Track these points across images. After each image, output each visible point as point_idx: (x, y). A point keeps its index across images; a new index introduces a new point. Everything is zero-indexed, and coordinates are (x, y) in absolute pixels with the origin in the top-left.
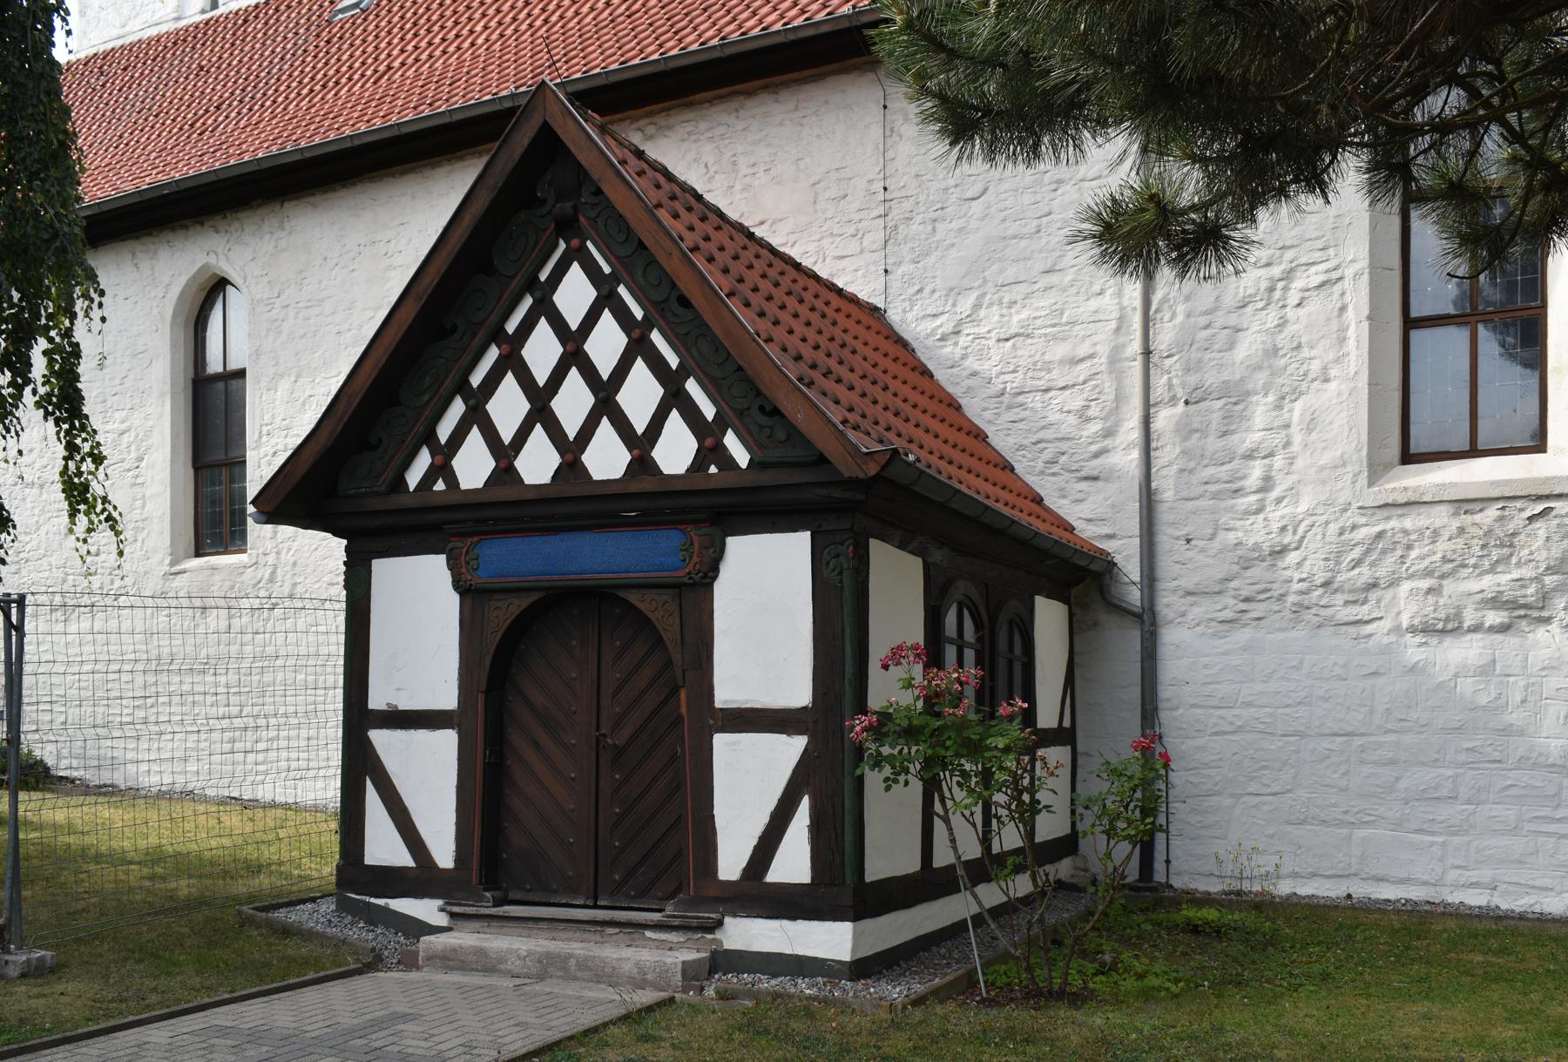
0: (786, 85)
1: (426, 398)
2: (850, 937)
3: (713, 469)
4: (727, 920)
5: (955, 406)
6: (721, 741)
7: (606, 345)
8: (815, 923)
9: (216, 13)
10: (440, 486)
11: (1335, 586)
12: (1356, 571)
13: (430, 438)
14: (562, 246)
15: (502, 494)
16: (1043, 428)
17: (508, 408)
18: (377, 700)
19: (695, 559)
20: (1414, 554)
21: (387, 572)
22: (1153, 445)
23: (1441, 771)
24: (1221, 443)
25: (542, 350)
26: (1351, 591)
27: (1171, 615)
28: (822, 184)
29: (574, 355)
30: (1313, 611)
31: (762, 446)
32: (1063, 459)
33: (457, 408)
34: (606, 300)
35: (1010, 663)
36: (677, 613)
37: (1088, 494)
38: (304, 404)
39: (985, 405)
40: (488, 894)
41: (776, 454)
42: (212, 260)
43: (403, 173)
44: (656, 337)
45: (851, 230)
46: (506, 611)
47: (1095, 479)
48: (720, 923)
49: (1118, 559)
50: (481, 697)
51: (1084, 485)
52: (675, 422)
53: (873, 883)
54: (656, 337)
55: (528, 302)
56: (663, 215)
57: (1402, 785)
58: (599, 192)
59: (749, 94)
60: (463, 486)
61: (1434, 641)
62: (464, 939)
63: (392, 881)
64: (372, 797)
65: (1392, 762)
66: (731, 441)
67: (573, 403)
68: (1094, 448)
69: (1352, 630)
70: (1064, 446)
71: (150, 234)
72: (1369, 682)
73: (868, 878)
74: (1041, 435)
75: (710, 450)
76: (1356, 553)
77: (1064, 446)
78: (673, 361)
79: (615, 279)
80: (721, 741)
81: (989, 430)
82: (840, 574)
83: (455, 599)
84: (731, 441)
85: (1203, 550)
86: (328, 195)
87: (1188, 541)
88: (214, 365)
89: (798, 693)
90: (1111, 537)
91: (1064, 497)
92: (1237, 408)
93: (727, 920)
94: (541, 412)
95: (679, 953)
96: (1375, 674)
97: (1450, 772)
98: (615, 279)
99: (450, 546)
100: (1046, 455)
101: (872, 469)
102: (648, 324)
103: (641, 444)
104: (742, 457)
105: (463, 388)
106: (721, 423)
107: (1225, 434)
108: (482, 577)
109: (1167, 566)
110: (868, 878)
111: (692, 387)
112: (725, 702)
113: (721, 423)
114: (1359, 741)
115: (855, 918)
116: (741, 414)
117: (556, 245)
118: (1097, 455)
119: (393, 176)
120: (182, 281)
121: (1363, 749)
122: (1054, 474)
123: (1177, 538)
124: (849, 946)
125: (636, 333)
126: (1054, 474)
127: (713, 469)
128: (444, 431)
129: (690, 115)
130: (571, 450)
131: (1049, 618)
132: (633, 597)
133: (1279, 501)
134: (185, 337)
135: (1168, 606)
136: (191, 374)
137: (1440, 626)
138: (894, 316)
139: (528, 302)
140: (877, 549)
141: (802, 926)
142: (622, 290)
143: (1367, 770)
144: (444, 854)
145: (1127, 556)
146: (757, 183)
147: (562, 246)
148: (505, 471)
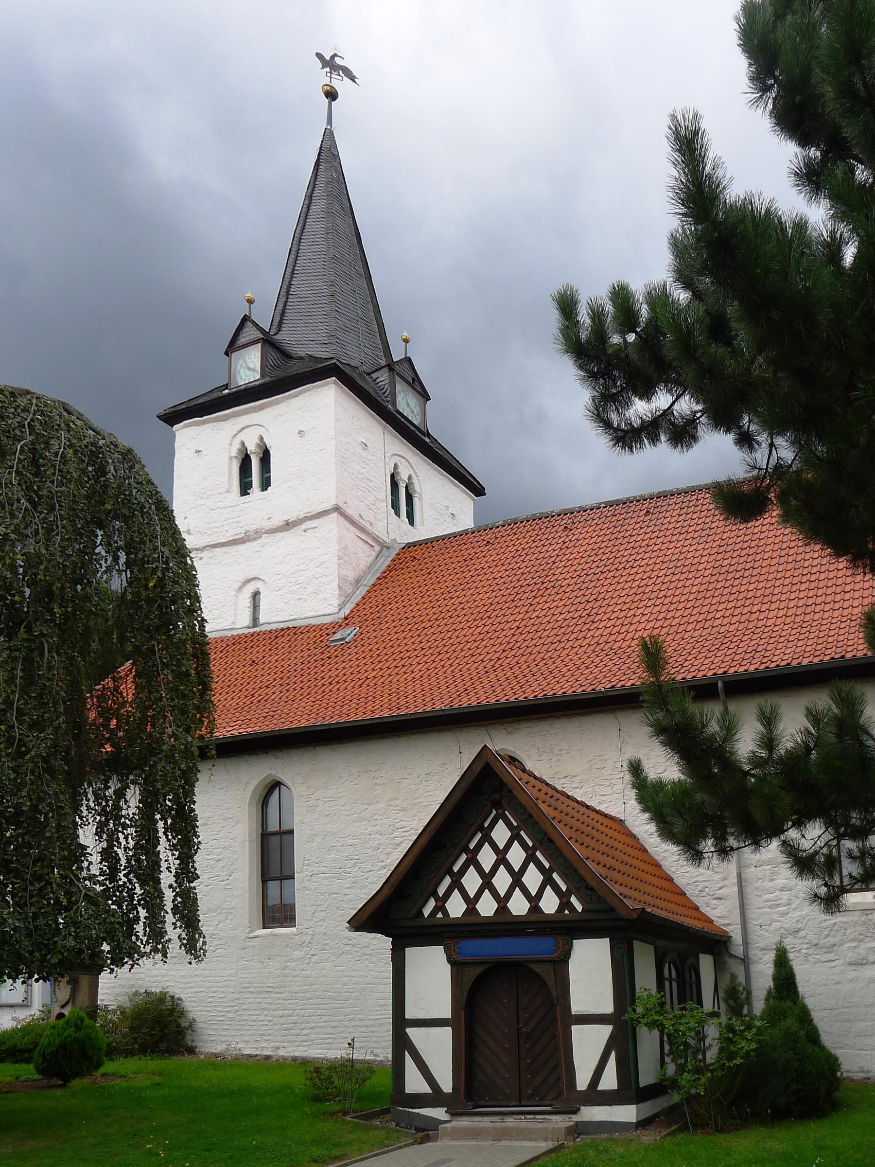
0: (575, 715)
1: (433, 876)
2: (635, 1111)
3: (567, 912)
4: (582, 1108)
5: (658, 866)
6: (574, 1028)
7: (516, 855)
8: (620, 1106)
9: (257, 629)
10: (440, 915)
11: (819, 946)
12: (827, 940)
13: (434, 894)
14: (494, 812)
15: (471, 920)
16: (697, 876)
17: (472, 881)
18: (410, 1014)
19: (560, 950)
20: (848, 932)
21: (413, 954)
22: (743, 884)
23: (867, 1023)
24: (771, 884)
25: (487, 857)
26: (826, 948)
27: (757, 959)
28: (593, 762)
29: (502, 860)
30: (813, 956)
31: (587, 903)
32: (707, 890)
33: (447, 881)
34: (515, 837)
35: (691, 985)
36: (553, 974)
37: (718, 905)
38: (329, 850)
39: (671, 865)
40: (470, 1104)
41: (592, 907)
42: (274, 772)
43: (383, 738)
44: (538, 854)
45: (608, 783)
46: (473, 973)
47: (721, 899)
48: (579, 1109)
49: (731, 934)
50: (463, 1012)
51: (715, 902)
52: (549, 890)
53: (645, 1087)
54: (538, 854)
55: (479, 835)
56: (540, 803)
57: (852, 1030)
58: (510, 791)
59: (557, 717)
60: (451, 916)
61: (859, 967)
62: (463, 1122)
63: (419, 1100)
64: (408, 1060)
65: (848, 1021)
66: (573, 900)
67: (502, 881)
68: (719, 885)
69: (828, 964)
70: (707, 884)
71: (236, 756)
72: (836, 986)
73: (641, 1085)
74: (697, 879)
75: (565, 904)
76: (826, 932)
77: (707, 884)
78: (547, 865)
79: (534, 848)
80: (574, 1028)
81: (674, 876)
82: (622, 956)
83: (448, 967)
84: (573, 900)
85: (767, 931)
86: (340, 745)
87: (761, 926)
88: (273, 826)
89: (608, 1008)
90: (729, 924)
91: (708, 907)
92: (776, 869)
93: (582, 1108)
94: (487, 883)
95: (561, 1122)
96: (838, 983)
97: (870, 1024)
98: (518, 828)
99: (446, 942)
100: (699, 888)
101: (635, 916)
102: (534, 848)
103: (534, 900)
104: (579, 908)
105: (450, 872)
106: (569, 893)
107: (772, 880)
108: (459, 958)
109: (753, 937)
110: (641, 1085)
111: (555, 876)
112: (576, 1012)
113: (569, 893)
114: (835, 1012)
115: (636, 1104)
116: (578, 889)
117: (491, 812)
118: (721, 888)
119: (377, 739)
120: (256, 782)
121: (836, 1015)
122: (703, 897)
123: (756, 925)
124: (635, 1115)
125: (530, 852)
126: (703, 897)
127: (567, 912)
128: (441, 891)
129: (529, 724)
130: (503, 902)
131: (706, 963)
132: (533, 966)
133: (795, 909)
134: (256, 811)
135: (755, 955)
136: (260, 832)
137: (861, 962)
138: (629, 824)
139: (479, 835)
140: (636, 944)
141: (615, 1108)
142: (522, 833)
143: (839, 1024)
144: (447, 1086)
145: (735, 933)
146: (563, 758)
147: (494, 812)
148: (471, 910)
